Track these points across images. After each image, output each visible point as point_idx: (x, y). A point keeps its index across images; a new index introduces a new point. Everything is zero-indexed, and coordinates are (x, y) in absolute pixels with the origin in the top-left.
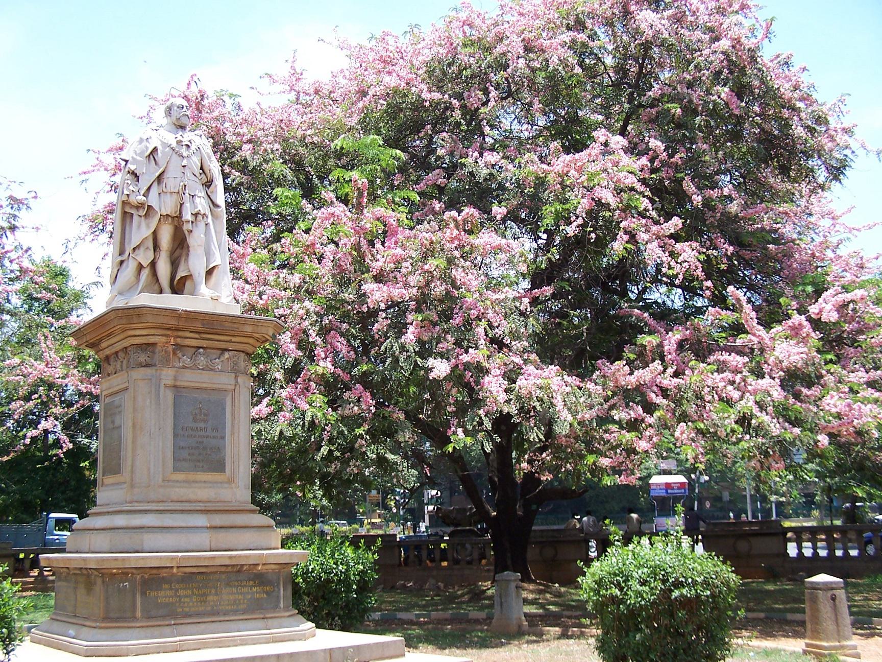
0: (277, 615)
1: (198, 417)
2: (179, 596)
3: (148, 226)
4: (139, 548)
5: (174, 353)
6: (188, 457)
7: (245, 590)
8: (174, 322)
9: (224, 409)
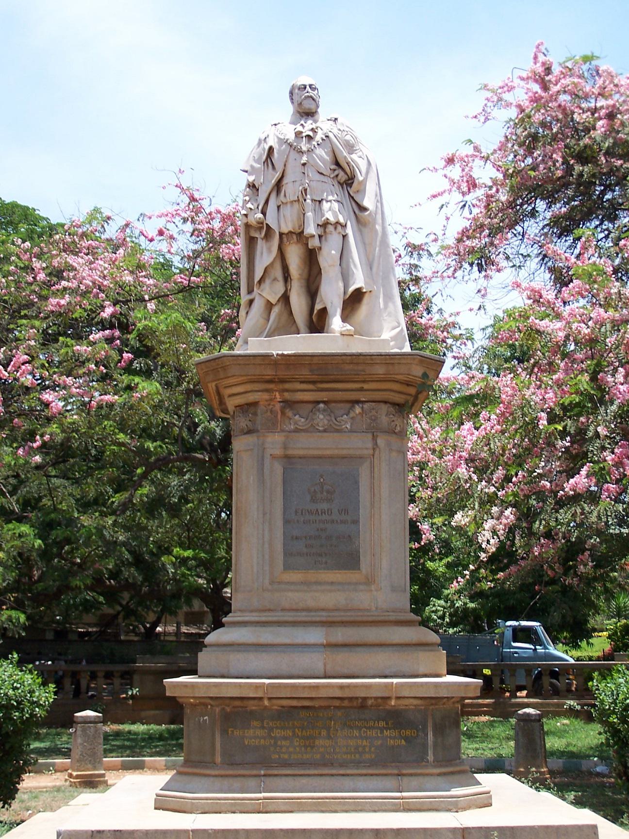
0: (419, 771)
1: (319, 496)
2: (275, 738)
3: (269, 250)
4: (224, 671)
5: (283, 413)
6: (305, 550)
7: (373, 733)
8: (269, 372)
9: (357, 483)
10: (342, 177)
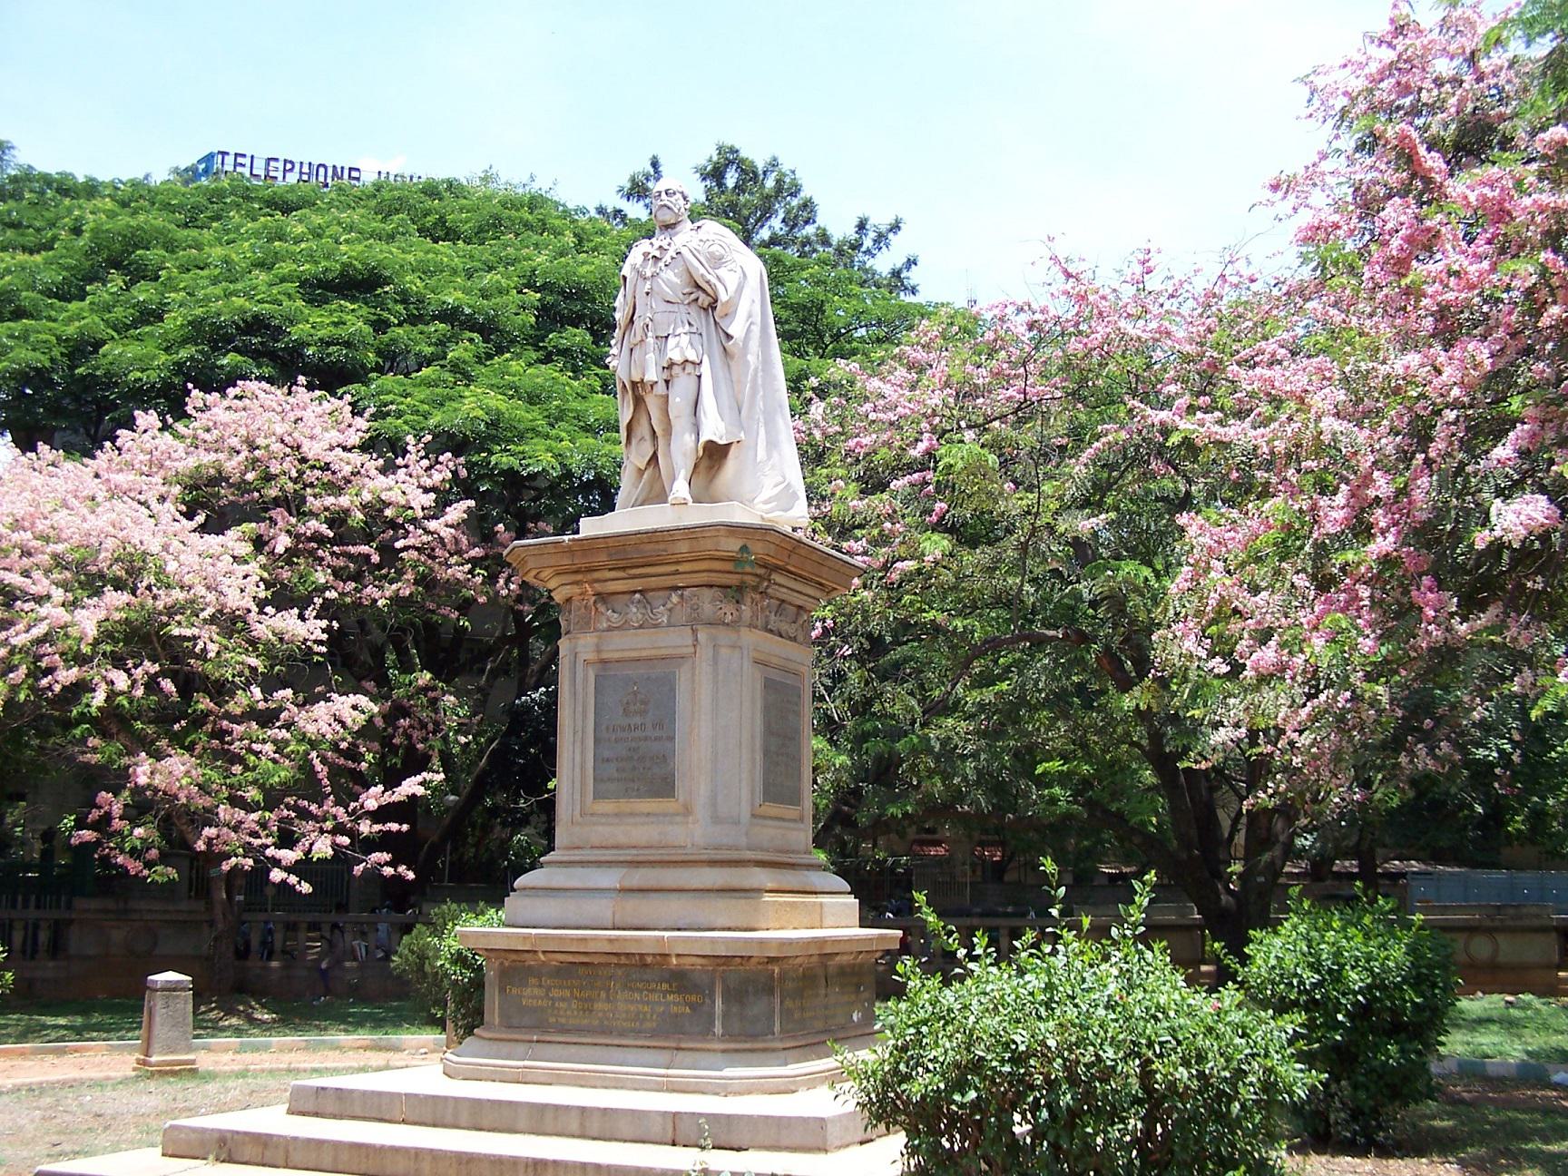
0: (708, 1046)
1: (632, 708)
7: (655, 997)
9: (673, 690)
10: (704, 300)
